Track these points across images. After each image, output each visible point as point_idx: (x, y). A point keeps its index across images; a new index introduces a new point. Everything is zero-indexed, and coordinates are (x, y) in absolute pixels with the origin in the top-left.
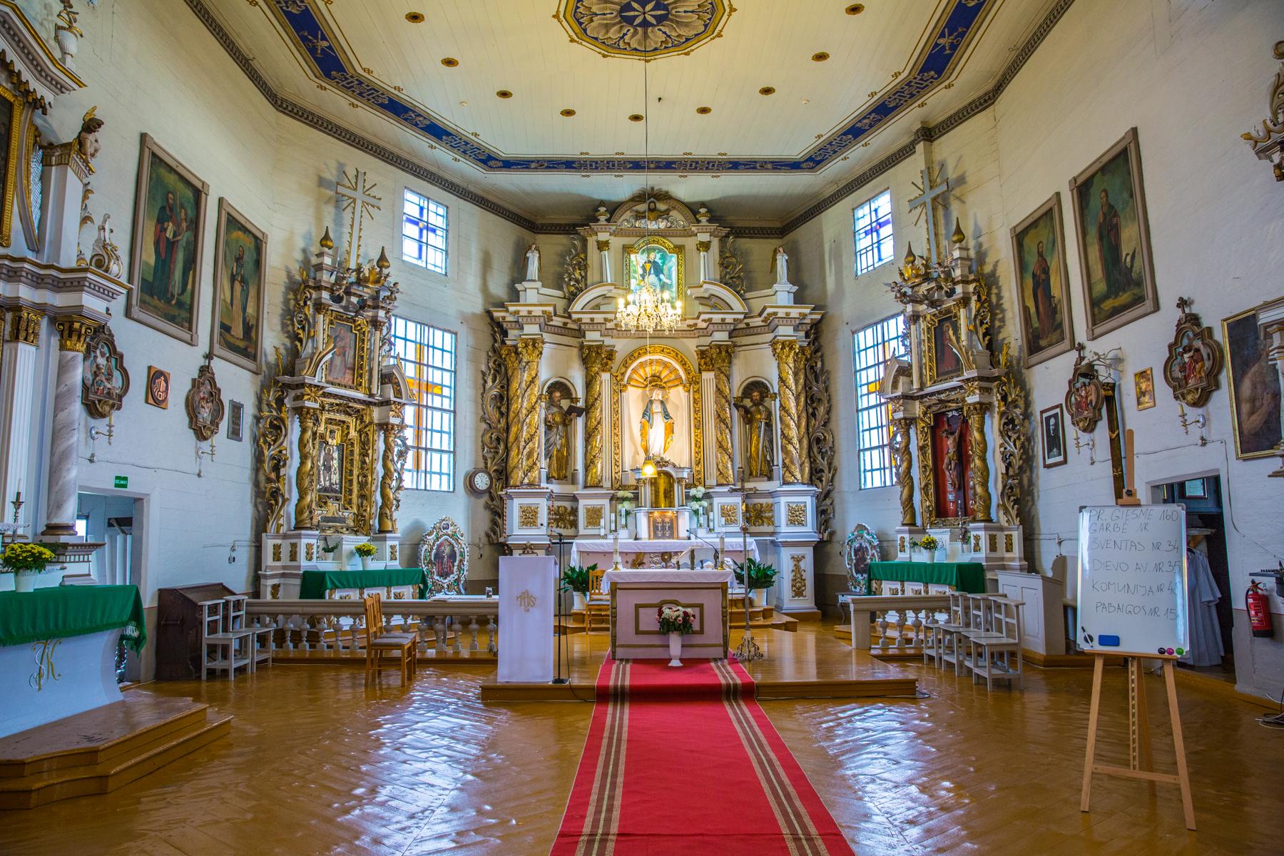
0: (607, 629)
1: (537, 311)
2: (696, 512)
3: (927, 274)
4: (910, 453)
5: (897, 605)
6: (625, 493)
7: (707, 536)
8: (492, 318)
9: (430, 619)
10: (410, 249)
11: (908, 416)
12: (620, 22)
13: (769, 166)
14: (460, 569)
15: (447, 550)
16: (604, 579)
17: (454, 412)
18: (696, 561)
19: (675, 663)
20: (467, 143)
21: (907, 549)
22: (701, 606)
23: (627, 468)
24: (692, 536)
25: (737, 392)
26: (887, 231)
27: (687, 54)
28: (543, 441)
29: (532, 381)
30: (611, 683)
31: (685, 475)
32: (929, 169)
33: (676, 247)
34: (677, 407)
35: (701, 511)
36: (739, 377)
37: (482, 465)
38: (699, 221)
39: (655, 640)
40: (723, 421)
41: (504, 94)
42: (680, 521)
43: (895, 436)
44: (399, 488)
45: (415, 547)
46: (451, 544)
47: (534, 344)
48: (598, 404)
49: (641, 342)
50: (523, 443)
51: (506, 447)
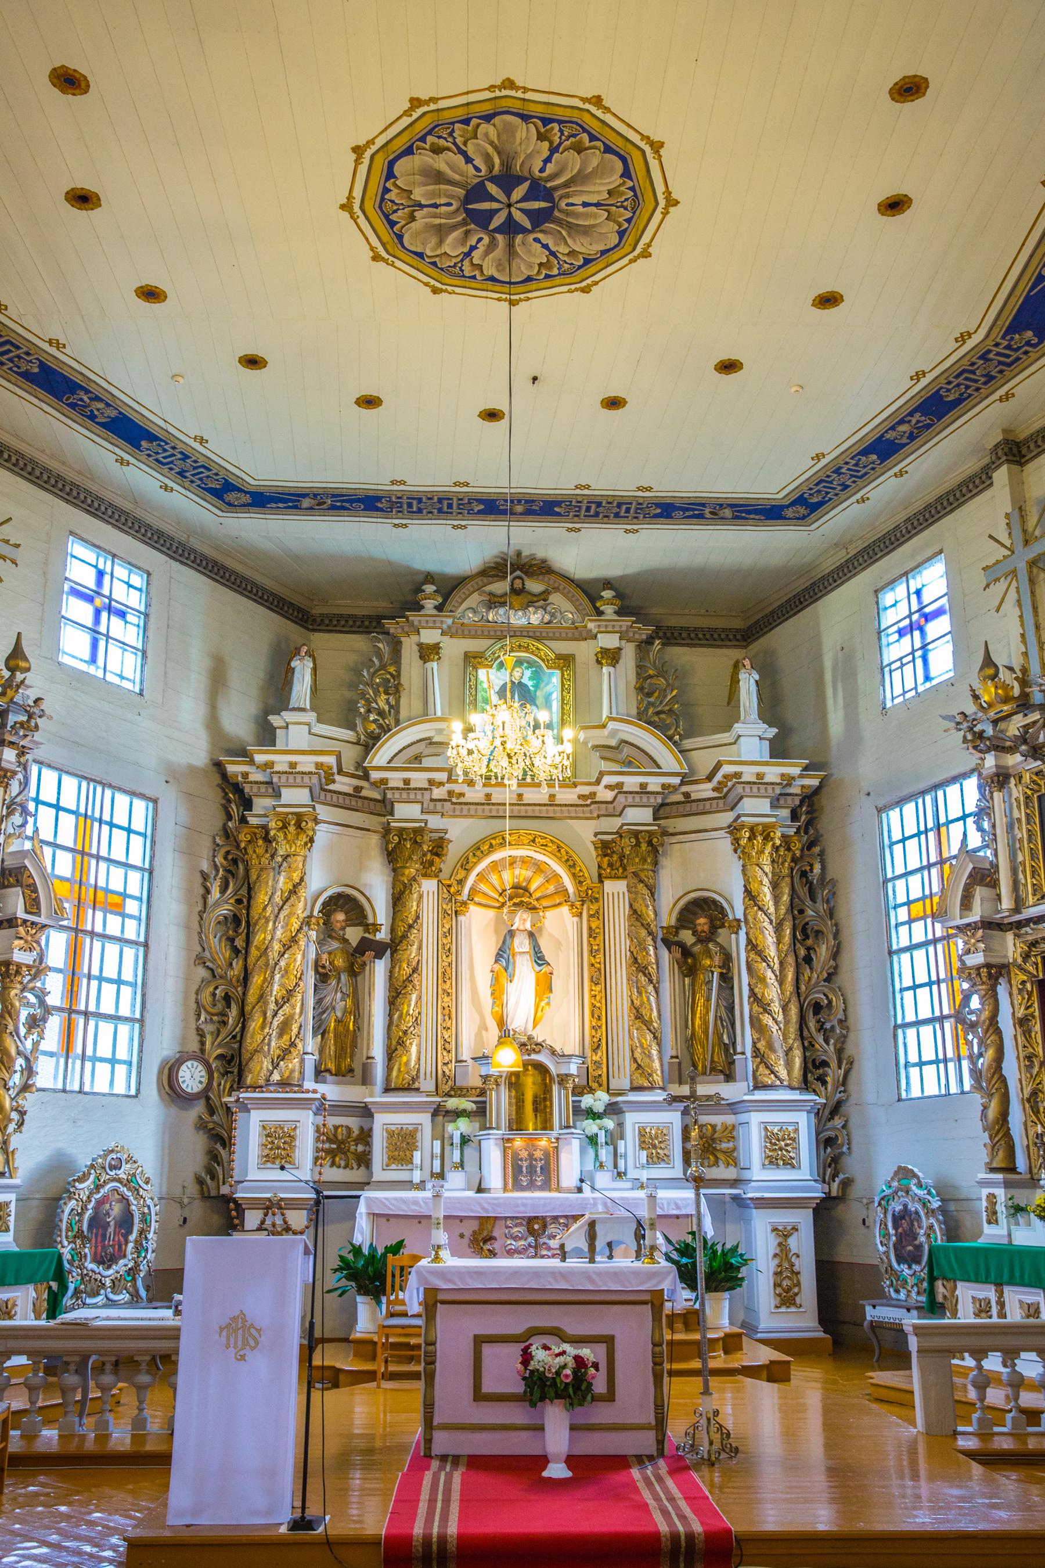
0: (415, 1376)
1: (306, 763)
2: (593, 1140)
3: (1025, 696)
4: (998, 1032)
5: (1001, 1341)
6: (461, 1102)
7: (618, 1185)
8: (224, 775)
9: (53, 1365)
10: (74, 644)
11: (993, 961)
12: (464, 223)
13: (727, 513)
14: (139, 1247)
15: (116, 1210)
16: (413, 1281)
17: (146, 945)
18: (600, 1244)
19: (557, 1470)
20: (185, 457)
21: (1002, 1217)
22: (608, 1341)
23: (466, 1055)
24: (586, 1187)
25: (668, 917)
26: (939, 627)
27: (586, 290)
28: (311, 1002)
29: (294, 891)
30: (418, 1530)
31: (573, 1069)
32: (1021, 509)
33: (559, 657)
34: (558, 944)
35: (602, 1138)
36: (672, 889)
37: (194, 1046)
38: (600, 613)
39: (515, 1414)
40: (643, 970)
41: (253, 362)
42: (564, 1157)
43: (967, 998)
44: (26, 1088)
45: (53, 1205)
46: (124, 1199)
47: (299, 823)
48: (413, 935)
49: (494, 825)
50: (272, 1006)
51: (242, 1013)
